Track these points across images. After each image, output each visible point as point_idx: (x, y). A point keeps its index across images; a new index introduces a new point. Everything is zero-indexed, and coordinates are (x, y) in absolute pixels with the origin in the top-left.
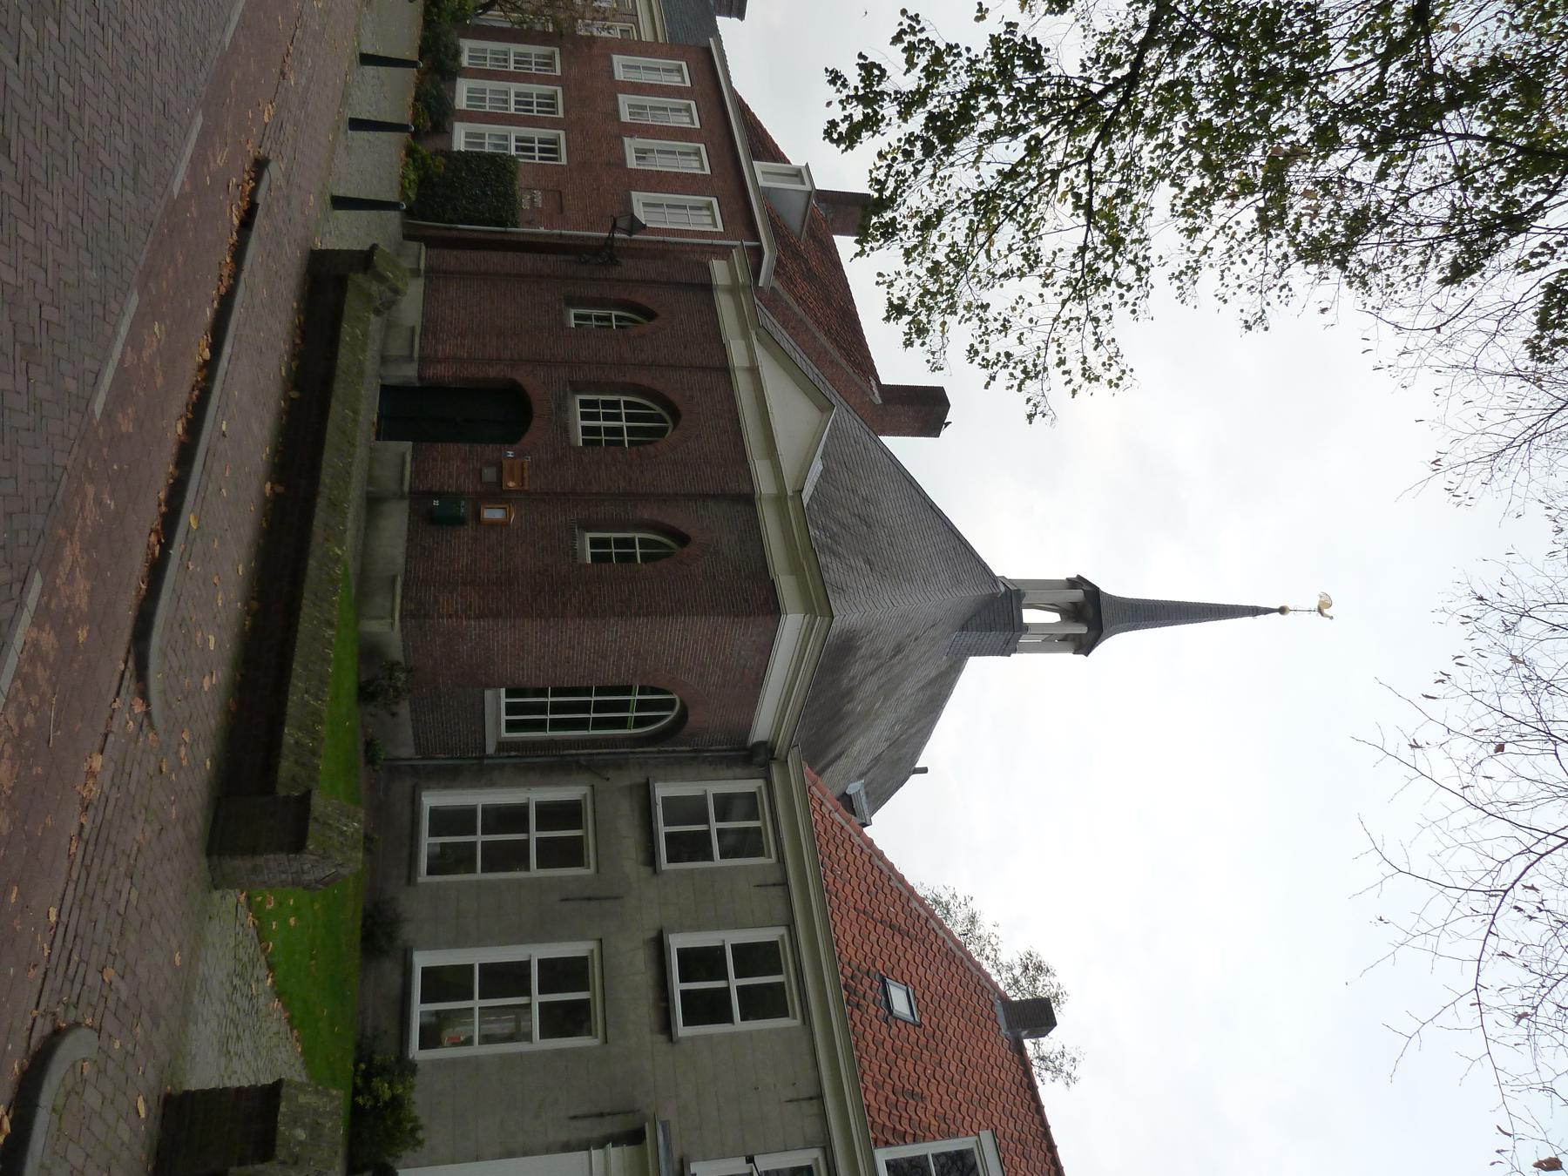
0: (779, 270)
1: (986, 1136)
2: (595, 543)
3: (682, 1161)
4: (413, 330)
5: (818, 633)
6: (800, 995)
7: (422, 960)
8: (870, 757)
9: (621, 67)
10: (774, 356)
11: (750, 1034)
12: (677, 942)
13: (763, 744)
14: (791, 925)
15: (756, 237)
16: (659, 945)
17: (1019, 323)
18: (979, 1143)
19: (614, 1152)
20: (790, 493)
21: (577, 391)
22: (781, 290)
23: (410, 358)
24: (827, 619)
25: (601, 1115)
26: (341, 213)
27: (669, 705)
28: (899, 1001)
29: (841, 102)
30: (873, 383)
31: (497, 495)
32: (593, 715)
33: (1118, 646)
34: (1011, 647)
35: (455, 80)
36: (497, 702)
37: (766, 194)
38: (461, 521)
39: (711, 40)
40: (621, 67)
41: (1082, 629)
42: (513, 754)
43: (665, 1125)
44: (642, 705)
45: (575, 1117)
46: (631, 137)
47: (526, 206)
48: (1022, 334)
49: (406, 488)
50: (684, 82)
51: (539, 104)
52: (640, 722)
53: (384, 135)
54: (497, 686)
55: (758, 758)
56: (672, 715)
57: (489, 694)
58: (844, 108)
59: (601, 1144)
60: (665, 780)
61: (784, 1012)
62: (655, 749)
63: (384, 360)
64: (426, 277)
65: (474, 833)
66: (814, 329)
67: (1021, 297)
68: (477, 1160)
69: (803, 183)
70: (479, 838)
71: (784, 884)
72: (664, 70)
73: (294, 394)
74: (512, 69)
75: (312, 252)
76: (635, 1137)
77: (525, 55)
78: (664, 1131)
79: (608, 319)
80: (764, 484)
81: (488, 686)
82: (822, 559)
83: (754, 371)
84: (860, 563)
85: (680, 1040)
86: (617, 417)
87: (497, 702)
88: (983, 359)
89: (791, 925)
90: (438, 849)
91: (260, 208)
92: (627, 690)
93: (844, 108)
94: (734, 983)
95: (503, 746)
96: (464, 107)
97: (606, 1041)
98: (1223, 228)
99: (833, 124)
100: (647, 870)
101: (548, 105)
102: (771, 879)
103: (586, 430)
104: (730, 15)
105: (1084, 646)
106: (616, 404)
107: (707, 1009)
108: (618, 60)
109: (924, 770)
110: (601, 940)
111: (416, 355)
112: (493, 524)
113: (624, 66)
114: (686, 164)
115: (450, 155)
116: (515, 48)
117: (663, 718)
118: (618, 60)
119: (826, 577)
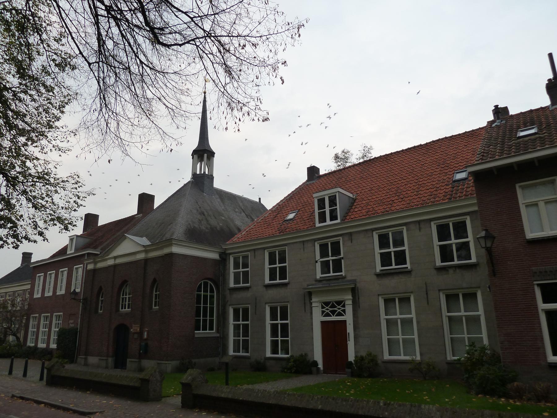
0: (95, 248)
1: (314, 195)
2: (155, 306)
3: (316, 281)
4: (100, 359)
5: (177, 242)
6: (279, 247)
7: (269, 354)
8: (247, 219)
9: (37, 295)
10: (112, 251)
11: (409, 244)
12: (267, 281)
13: (220, 256)
14: (264, 249)
15: (84, 254)
16: (320, 281)
17: (67, 199)
18: (316, 197)
19: (313, 300)
20: (144, 249)
21: (119, 310)
22: (102, 247)
23: (107, 360)
24: (173, 240)
25: (305, 303)
26: (13, 372)
27: (206, 284)
28: (291, 216)
29: (8, 245)
30: (136, 216)
31: (141, 333)
32: (208, 305)
33: (213, 144)
34: (210, 177)
35: (38, 348)
36: (200, 333)
37: (77, 250)
38: (147, 345)
39: (31, 266)
40: (37, 295)
41: (206, 155)
42: (220, 328)
43: (308, 285)
44: (206, 291)
45: (305, 311)
46: (56, 292)
47: (73, 325)
48: (70, 198)
49: (137, 360)
50: (66, 270)
51: (59, 321)
52: (212, 291)
53: (14, 363)
54: (194, 334)
55: (224, 256)
56: (209, 282)
57: (196, 336)
58: (10, 244)
59: (311, 304)
60: (229, 284)
61: (402, 232)
62: (221, 287)
63: (107, 367)
64: (88, 356)
65: (278, 340)
66: (115, 236)
67: (60, 198)
68: (313, 338)
69: (74, 238)
70: (241, 338)
71: (254, 250)
72: (62, 277)
73: (75, 387)
74: (47, 330)
75: (46, 385)
76: (310, 294)
77: (43, 325)
78: (310, 286)
79: (102, 301)
80: (141, 256)
81: (194, 336)
82: (164, 239)
83: (115, 258)
84: (170, 227)
85: (477, 262)
86: (126, 298)
87: (200, 333)
88: (77, 207)
89: (264, 249)
90: (244, 350)
91: (21, 395)
92: (199, 296)
93: (10, 244)
94: (392, 249)
95: (218, 331)
96: (46, 345)
97: (412, 292)
98: (48, 142)
99: (13, 247)
100: (250, 290)
101: (59, 317)
102: (418, 225)
103: (128, 308)
104: (31, 258)
105: (211, 154)
106: (123, 299)
107: (401, 257)
108: (36, 296)
109: (260, 199)
110: (266, 303)
111: (106, 358)
112: (148, 335)
113: (37, 294)
114: (80, 272)
115: (58, 348)
116: (30, 329)
117: (210, 284)
118: (36, 296)
119: (168, 238)
